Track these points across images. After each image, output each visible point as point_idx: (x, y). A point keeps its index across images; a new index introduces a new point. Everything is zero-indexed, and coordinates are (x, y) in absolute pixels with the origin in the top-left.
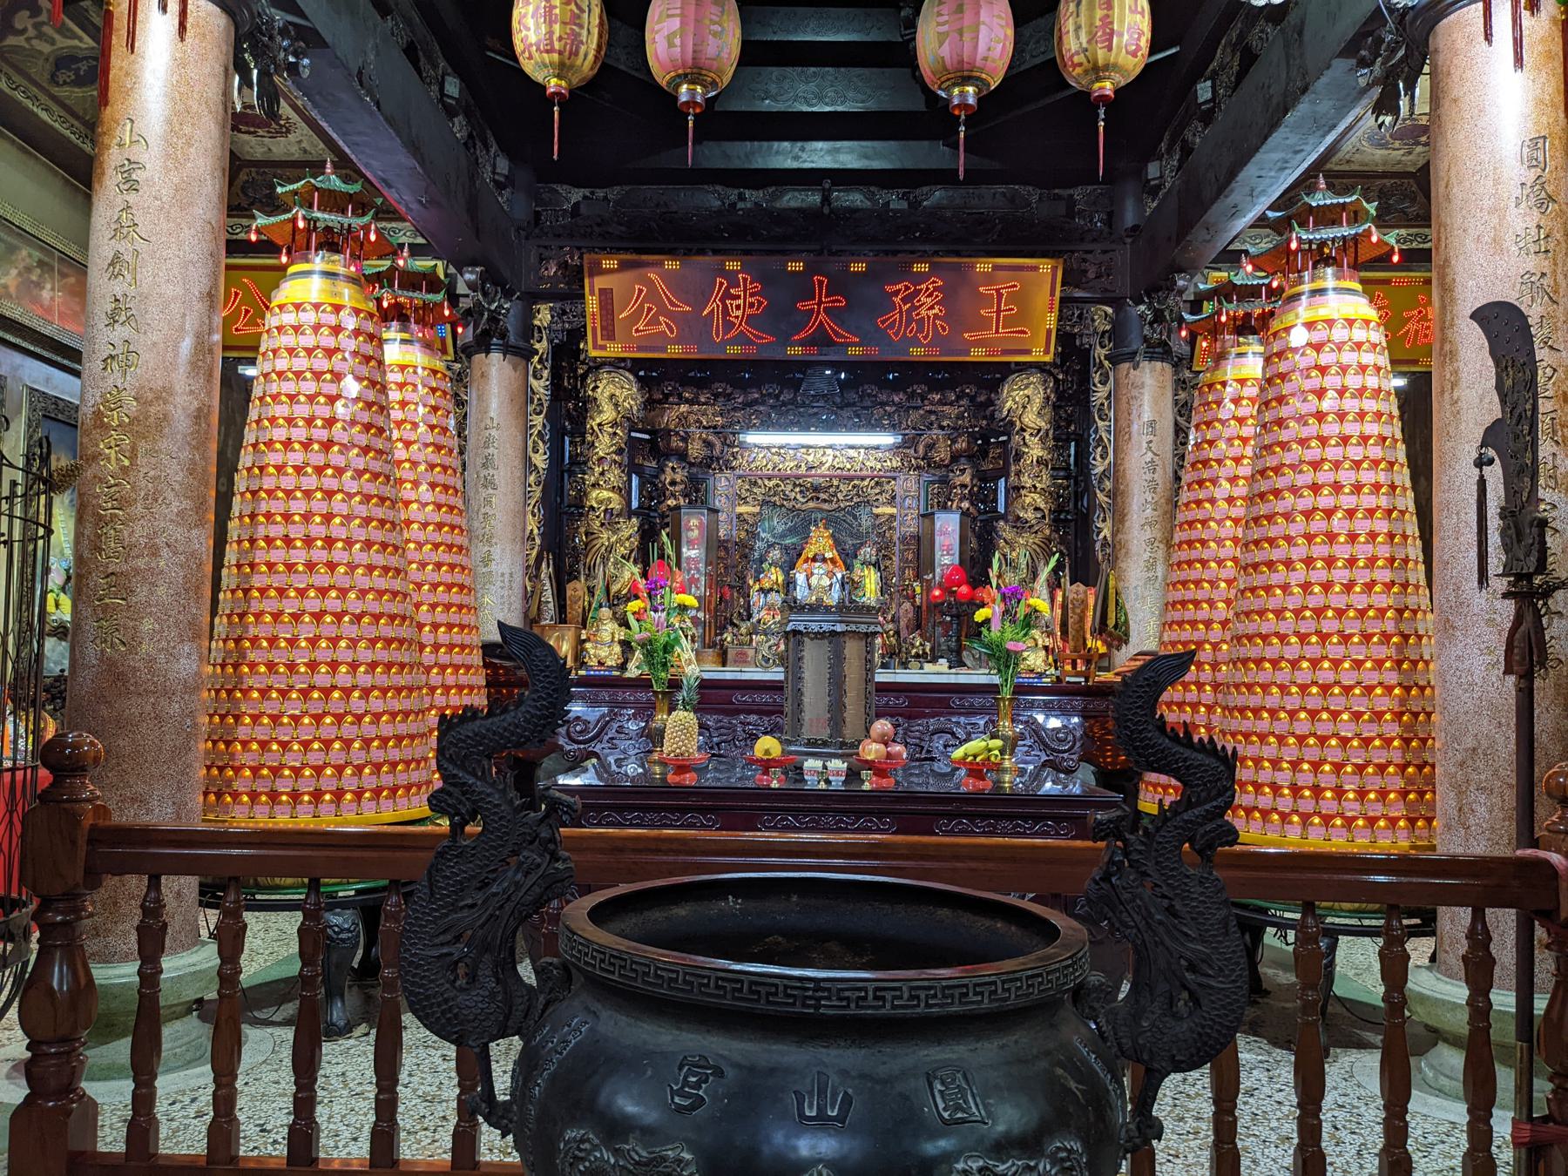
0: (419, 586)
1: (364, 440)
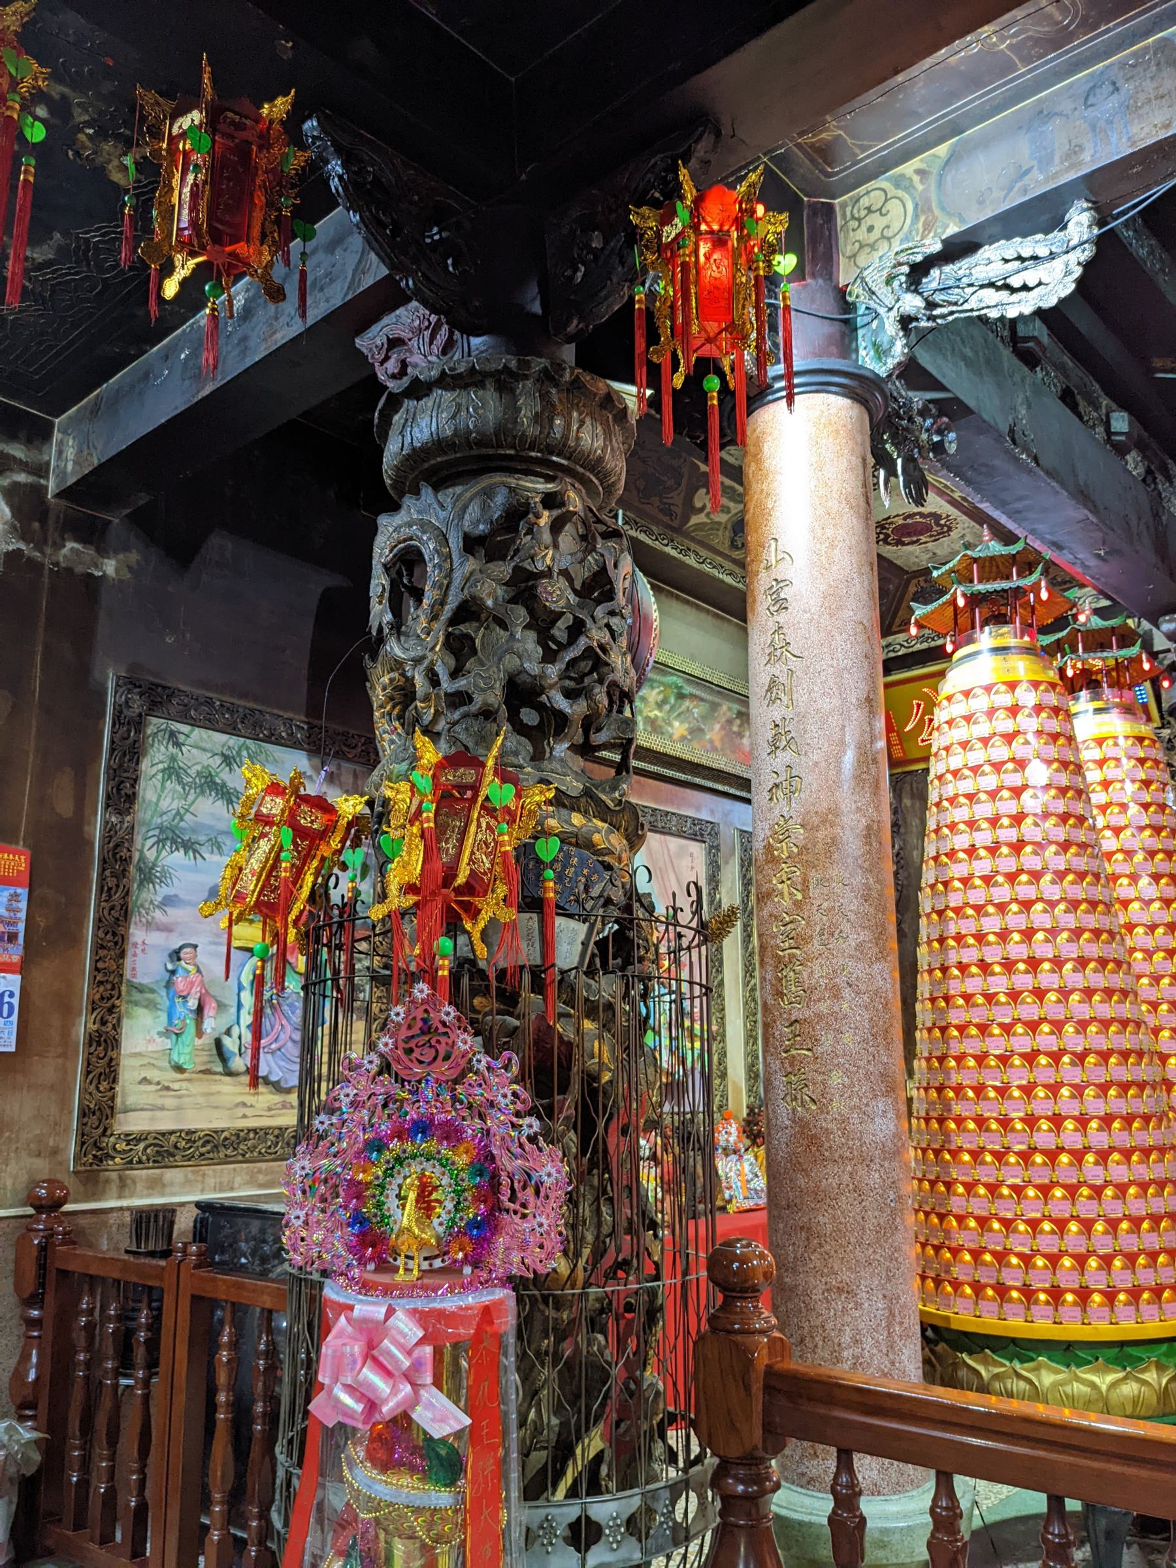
0: (1155, 1006)
1: (1061, 834)
